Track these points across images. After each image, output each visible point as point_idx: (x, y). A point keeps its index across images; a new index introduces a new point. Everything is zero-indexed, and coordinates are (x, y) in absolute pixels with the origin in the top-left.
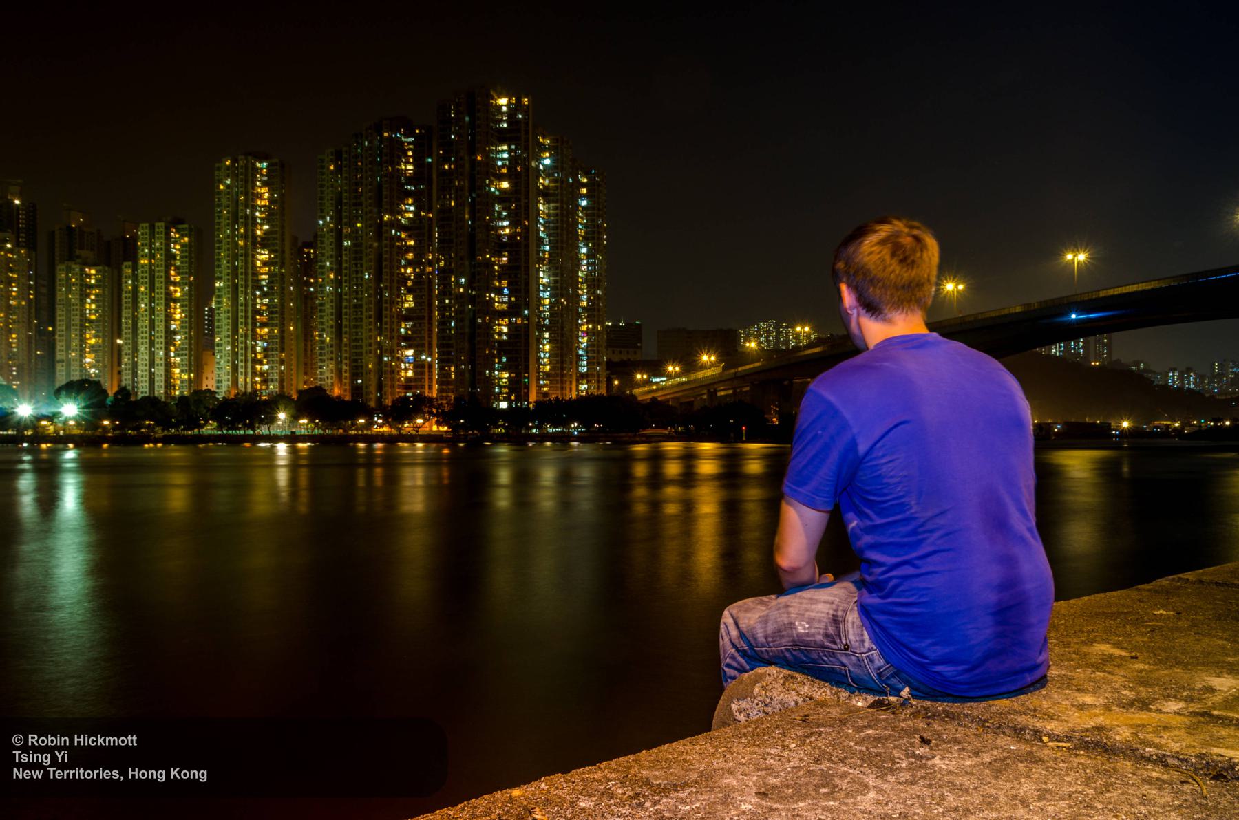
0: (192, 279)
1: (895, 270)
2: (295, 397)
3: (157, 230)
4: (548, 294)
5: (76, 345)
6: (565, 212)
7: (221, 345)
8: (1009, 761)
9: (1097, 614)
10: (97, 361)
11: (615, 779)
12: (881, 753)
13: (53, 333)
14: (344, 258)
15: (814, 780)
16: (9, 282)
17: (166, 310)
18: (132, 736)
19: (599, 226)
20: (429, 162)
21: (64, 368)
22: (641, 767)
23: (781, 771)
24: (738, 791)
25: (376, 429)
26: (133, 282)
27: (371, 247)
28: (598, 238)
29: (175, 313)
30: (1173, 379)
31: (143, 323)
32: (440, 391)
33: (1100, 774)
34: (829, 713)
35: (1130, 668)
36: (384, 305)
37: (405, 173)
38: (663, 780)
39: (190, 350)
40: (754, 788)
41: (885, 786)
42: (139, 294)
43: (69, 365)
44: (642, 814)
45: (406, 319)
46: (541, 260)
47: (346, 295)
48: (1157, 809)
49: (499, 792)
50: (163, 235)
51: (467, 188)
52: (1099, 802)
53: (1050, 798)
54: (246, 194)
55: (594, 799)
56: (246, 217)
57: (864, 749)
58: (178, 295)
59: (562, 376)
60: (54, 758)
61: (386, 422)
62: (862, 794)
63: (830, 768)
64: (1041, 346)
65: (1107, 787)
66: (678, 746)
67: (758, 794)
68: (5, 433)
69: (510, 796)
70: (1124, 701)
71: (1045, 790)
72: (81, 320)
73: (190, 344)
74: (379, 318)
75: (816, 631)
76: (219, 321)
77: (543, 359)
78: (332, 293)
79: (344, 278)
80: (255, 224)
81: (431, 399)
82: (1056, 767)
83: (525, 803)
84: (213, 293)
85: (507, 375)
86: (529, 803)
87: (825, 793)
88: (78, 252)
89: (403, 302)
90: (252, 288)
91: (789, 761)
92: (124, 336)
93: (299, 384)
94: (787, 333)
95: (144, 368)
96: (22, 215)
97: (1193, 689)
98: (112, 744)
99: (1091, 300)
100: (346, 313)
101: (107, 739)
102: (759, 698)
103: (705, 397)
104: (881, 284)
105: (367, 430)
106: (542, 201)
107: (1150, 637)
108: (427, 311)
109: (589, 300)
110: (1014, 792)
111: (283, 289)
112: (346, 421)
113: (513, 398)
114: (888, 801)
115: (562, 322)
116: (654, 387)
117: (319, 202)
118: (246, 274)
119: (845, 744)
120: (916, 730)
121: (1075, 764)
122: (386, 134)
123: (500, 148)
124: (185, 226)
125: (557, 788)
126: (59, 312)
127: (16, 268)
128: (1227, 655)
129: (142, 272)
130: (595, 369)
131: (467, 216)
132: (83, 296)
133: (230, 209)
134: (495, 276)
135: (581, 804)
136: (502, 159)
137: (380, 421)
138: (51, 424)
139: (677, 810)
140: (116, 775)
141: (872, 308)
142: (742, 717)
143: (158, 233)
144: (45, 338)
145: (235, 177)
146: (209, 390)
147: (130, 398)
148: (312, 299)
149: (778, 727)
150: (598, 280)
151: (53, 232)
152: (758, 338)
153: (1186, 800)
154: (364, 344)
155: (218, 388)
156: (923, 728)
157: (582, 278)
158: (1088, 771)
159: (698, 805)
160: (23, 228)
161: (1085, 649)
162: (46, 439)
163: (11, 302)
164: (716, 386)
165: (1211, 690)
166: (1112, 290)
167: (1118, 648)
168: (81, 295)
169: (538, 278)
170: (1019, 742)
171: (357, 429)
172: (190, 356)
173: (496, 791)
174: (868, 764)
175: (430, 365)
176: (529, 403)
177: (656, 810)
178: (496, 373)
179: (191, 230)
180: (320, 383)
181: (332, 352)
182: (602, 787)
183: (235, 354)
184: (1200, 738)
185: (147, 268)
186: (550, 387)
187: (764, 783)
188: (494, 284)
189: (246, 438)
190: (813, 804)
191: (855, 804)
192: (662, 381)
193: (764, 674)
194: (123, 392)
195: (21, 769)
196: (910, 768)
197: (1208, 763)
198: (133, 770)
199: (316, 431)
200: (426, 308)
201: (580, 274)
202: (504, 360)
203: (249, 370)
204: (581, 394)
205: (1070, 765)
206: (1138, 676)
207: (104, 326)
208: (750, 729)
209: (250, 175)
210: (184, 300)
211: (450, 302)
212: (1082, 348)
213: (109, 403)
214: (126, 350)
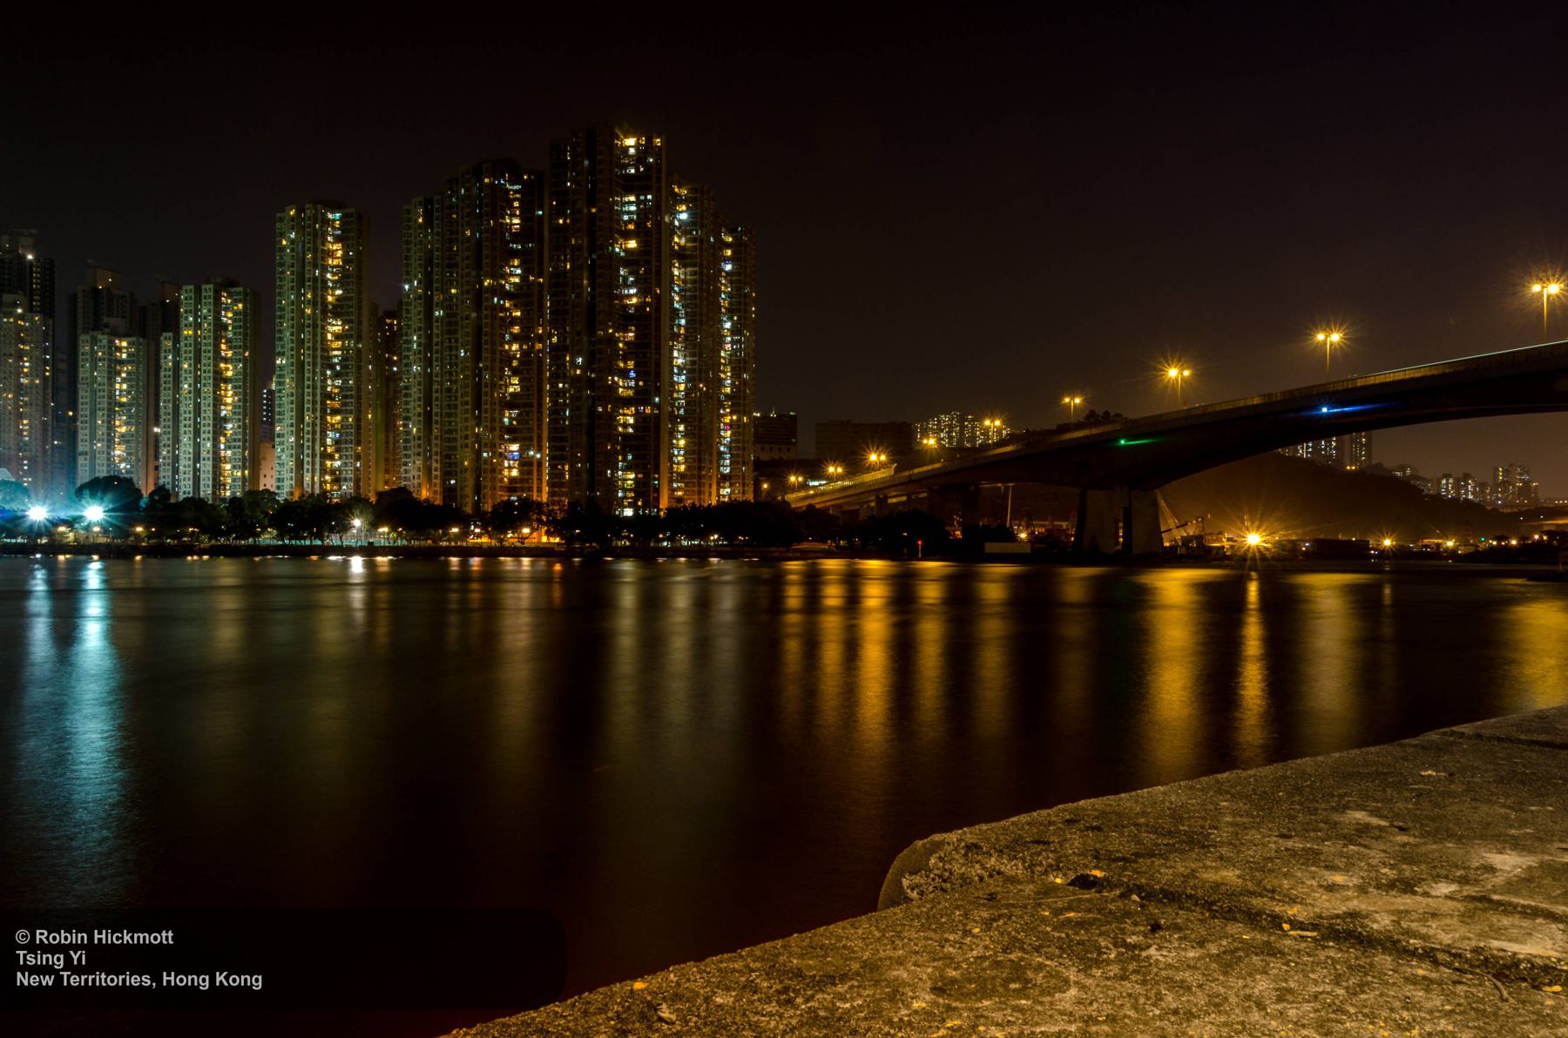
0: (247, 354)
2: (373, 499)
3: (204, 294)
4: (683, 377)
7: (283, 436)
8: (1241, 954)
10: (128, 454)
11: (758, 970)
13: (74, 419)
14: (435, 331)
16: (20, 356)
17: (215, 392)
18: (167, 932)
19: (745, 296)
20: (539, 216)
21: (87, 462)
22: (791, 954)
25: (472, 540)
26: (174, 357)
30: (1447, 488)
31: (186, 407)
32: (552, 494)
33: (1353, 970)
34: (1021, 890)
35: (1391, 841)
36: (484, 390)
37: (511, 229)
38: (818, 971)
39: (245, 441)
40: (929, 982)
41: (1089, 982)
42: (182, 372)
43: (93, 458)
44: (791, 1012)
45: (511, 406)
46: (675, 337)
47: (437, 376)
48: (1423, 1015)
52: (1352, 1005)
54: (315, 251)
55: (734, 994)
56: (315, 279)
57: (1063, 935)
58: (230, 374)
59: (700, 477)
60: (68, 959)
61: (485, 531)
62: (1060, 992)
63: (1021, 959)
64: (1284, 445)
65: (1362, 987)
66: (837, 928)
68: (13, 541)
70: (1384, 881)
72: (109, 404)
73: (244, 434)
74: (478, 404)
76: (280, 405)
77: (677, 456)
79: (435, 356)
80: (325, 287)
81: (540, 504)
85: (632, 476)
87: (1015, 990)
88: (105, 319)
89: (507, 386)
90: (322, 366)
91: (972, 950)
92: (163, 423)
93: (378, 484)
94: (973, 428)
95: (187, 463)
97: (1469, 868)
98: (141, 942)
99: (1346, 391)
100: (437, 399)
101: (136, 935)
102: (936, 872)
103: (873, 504)
106: (677, 265)
107: (1416, 804)
109: (733, 384)
110: (1248, 991)
111: (359, 368)
112: (436, 529)
113: (640, 503)
116: (812, 492)
118: (315, 349)
119: (1040, 929)
123: (626, 199)
124: (240, 289)
125: (688, 980)
127: (29, 338)
128: (1511, 826)
129: (186, 346)
130: (740, 470)
131: (585, 282)
132: (112, 374)
134: (619, 355)
135: (718, 999)
136: (629, 213)
137: (478, 530)
138: (71, 531)
140: (146, 980)
142: (914, 895)
143: (205, 298)
145: (300, 229)
146: (267, 491)
149: (958, 908)
151: (75, 295)
153: (1459, 1005)
155: (278, 488)
156: (1136, 911)
157: (725, 358)
158: (1338, 967)
159: (860, 1002)
160: (36, 289)
161: (1335, 817)
162: (64, 549)
164: (886, 491)
165: (1491, 869)
168: (109, 372)
169: (672, 358)
170: (1253, 929)
171: (449, 540)
175: (540, 463)
176: (659, 510)
177: (810, 1008)
178: (620, 473)
179: (246, 294)
180: (403, 483)
182: (743, 979)
184: (1477, 928)
187: (941, 976)
188: (618, 366)
189: (312, 550)
190: (1000, 1002)
191: (1052, 1003)
192: (820, 485)
194: (161, 492)
195: (27, 973)
197: (1486, 959)
198: (169, 975)
200: (535, 393)
201: (723, 354)
202: (630, 457)
203: (317, 466)
204: (722, 499)
208: (924, 910)
214: (164, 440)
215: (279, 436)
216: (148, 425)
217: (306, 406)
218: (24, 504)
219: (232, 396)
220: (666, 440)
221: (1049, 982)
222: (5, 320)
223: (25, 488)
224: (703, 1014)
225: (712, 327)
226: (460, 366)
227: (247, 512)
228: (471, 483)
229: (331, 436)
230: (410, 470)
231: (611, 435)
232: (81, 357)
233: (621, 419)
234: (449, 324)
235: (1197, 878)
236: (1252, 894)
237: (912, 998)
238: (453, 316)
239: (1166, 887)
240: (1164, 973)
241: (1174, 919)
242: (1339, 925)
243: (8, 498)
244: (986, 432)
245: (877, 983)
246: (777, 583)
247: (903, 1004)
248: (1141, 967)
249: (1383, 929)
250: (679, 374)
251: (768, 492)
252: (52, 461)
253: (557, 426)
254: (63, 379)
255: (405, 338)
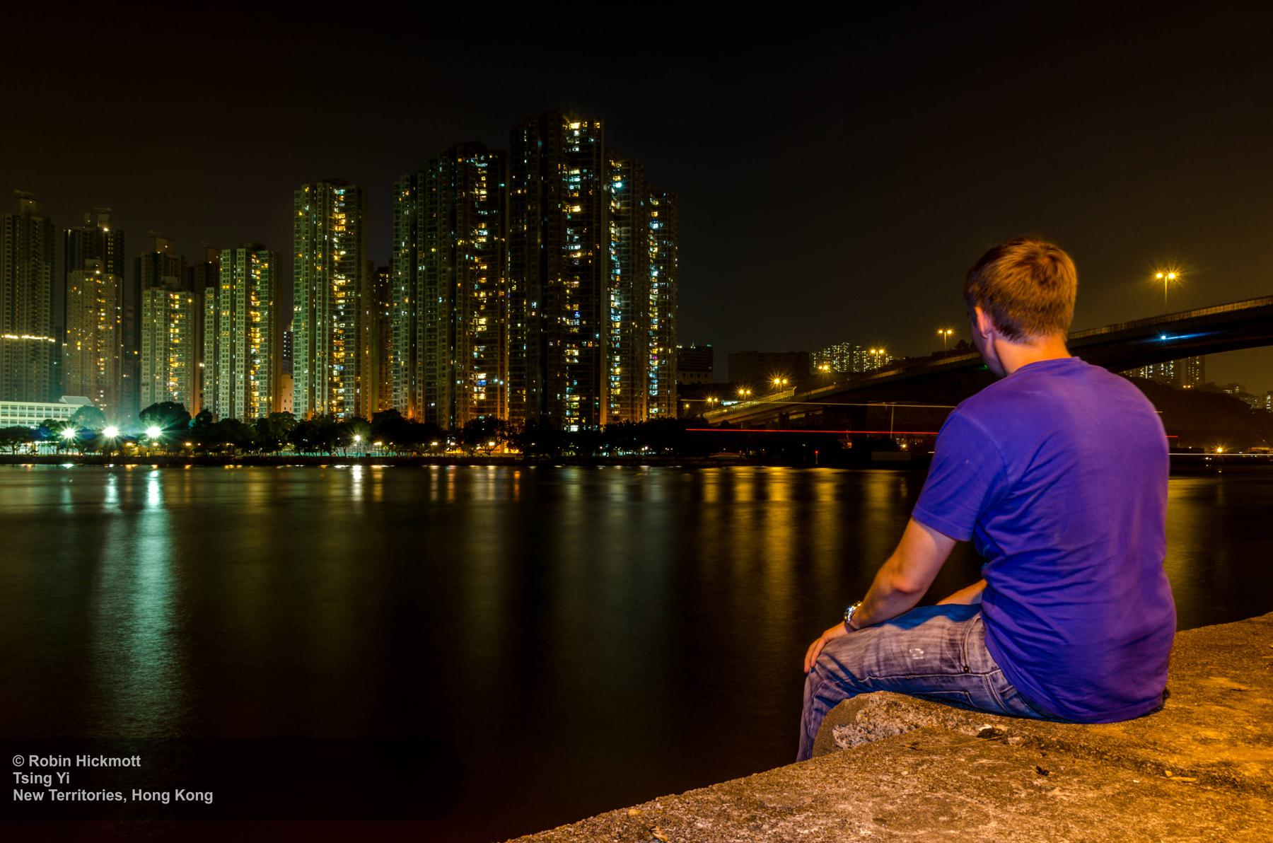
0: (271, 304)
1: (1037, 293)
2: (370, 419)
3: (238, 256)
4: (619, 317)
5: (160, 369)
6: (636, 236)
7: (299, 368)
8: (1132, 795)
9: (1210, 647)
10: (180, 384)
12: (996, 783)
13: (139, 357)
14: (419, 283)
15: (932, 808)
16: (98, 307)
17: (246, 334)
18: (136, 757)
20: (502, 187)
21: (149, 391)
22: (753, 790)
23: (897, 798)
24: (855, 817)
25: (448, 452)
26: (215, 307)
27: (445, 271)
28: (669, 261)
29: (255, 338)
31: (224, 347)
32: (512, 414)
33: (1231, 810)
34: (938, 741)
35: (1251, 703)
36: (458, 329)
37: (479, 198)
38: (778, 803)
39: (270, 373)
40: (871, 814)
42: (221, 319)
43: (153, 388)
44: (761, 836)
45: (479, 343)
46: (612, 284)
47: (420, 319)
49: (616, 811)
50: (244, 261)
51: (539, 213)
53: (1180, 833)
54: (324, 220)
55: (711, 820)
56: (324, 243)
57: (979, 778)
58: (258, 319)
59: (633, 399)
60: (55, 779)
61: (459, 445)
62: (983, 824)
65: (1241, 824)
67: (876, 820)
68: (93, 454)
69: (627, 815)
70: (1249, 736)
71: (1175, 825)
72: (165, 345)
73: (269, 368)
74: (453, 342)
75: (932, 656)
76: (297, 344)
77: (614, 382)
78: (407, 317)
79: (419, 302)
80: (332, 249)
81: (503, 422)
82: (1183, 801)
83: (643, 822)
84: (292, 318)
85: (577, 399)
86: (646, 822)
87: (944, 822)
88: (163, 278)
89: (476, 326)
90: (330, 313)
91: (904, 789)
92: (206, 360)
93: (371, 409)
95: (225, 391)
96: (111, 242)
98: (115, 765)
99: (1182, 321)
100: (420, 337)
101: (110, 760)
102: (862, 725)
103: (777, 420)
104: (1020, 307)
105: (441, 452)
106: (613, 225)
108: (499, 335)
109: (659, 322)
110: (1142, 826)
111: (359, 313)
112: (420, 443)
113: (584, 421)
114: (1011, 831)
115: (633, 344)
116: (725, 411)
117: (395, 227)
118: (324, 299)
119: (959, 773)
120: (1031, 761)
121: (1204, 800)
122: (460, 160)
123: (572, 172)
124: (266, 252)
125: (672, 808)
126: (144, 337)
127: (104, 294)
129: (224, 298)
130: (666, 392)
131: (539, 240)
132: (168, 320)
133: (309, 235)
134: (566, 299)
135: (699, 824)
136: (574, 183)
137: (453, 444)
138: (136, 446)
139: (796, 834)
140: (119, 796)
141: (1011, 331)
142: (844, 744)
143: (239, 259)
144: (131, 362)
145: (313, 203)
146: (287, 413)
147: (211, 420)
148: (387, 323)
149: (887, 754)
150: (670, 303)
151: (140, 259)
152: (831, 361)
154: (437, 368)
155: (296, 410)
157: (653, 301)
158: (1218, 807)
159: (816, 829)
160: (111, 255)
161: (1202, 682)
162: (131, 460)
163: (99, 327)
164: (788, 409)
166: (1205, 310)
167: (1236, 681)
168: (166, 320)
169: (610, 301)
170: (1142, 775)
171: (430, 452)
172: (269, 379)
173: (613, 810)
174: (986, 794)
175: (502, 389)
176: (600, 426)
177: (775, 833)
178: (567, 396)
179: (271, 256)
180: (394, 406)
181: (406, 376)
182: (717, 809)
183: (312, 377)
185: (229, 294)
186: (621, 411)
188: (565, 308)
189: (322, 460)
190: (933, 832)
192: (733, 405)
193: (867, 701)
194: (205, 415)
195: (22, 791)
196: (1029, 798)
198: (137, 792)
199: (391, 453)
200: (499, 332)
201: (651, 298)
202: (576, 383)
203: (326, 393)
205: (1198, 801)
206: (1262, 711)
207: (187, 350)
208: (859, 755)
209: (328, 201)
210: (263, 325)
211: (522, 325)
212: (1173, 370)
213: (192, 426)
214: (208, 373)
215: (296, 368)
216: (195, 362)
217: (317, 344)
218: (100, 425)
219: (259, 338)
220: (606, 367)
221: (972, 816)
222: (87, 280)
223: (101, 412)
224: (689, 836)
225: (642, 275)
226: (438, 310)
227: (271, 430)
228: (447, 405)
229: (337, 368)
230: (399, 395)
231: (560, 365)
232: (144, 308)
233: (568, 352)
234: (430, 277)
235: (1088, 732)
236: (1137, 745)
237: (859, 827)
238: (433, 271)
239: (1062, 739)
240: (1068, 810)
241: (1071, 766)
242: (1215, 772)
243: (89, 420)
244: (872, 359)
245: (828, 814)
246: (697, 487)
247: (852, 831)
248: (1048, 805)
249: (1254, 776)
250: (616, 314)
251: (690, 410)
252: (122, 391)
253: (517, 358)
254: (130, 325)
255: (395, 288)
